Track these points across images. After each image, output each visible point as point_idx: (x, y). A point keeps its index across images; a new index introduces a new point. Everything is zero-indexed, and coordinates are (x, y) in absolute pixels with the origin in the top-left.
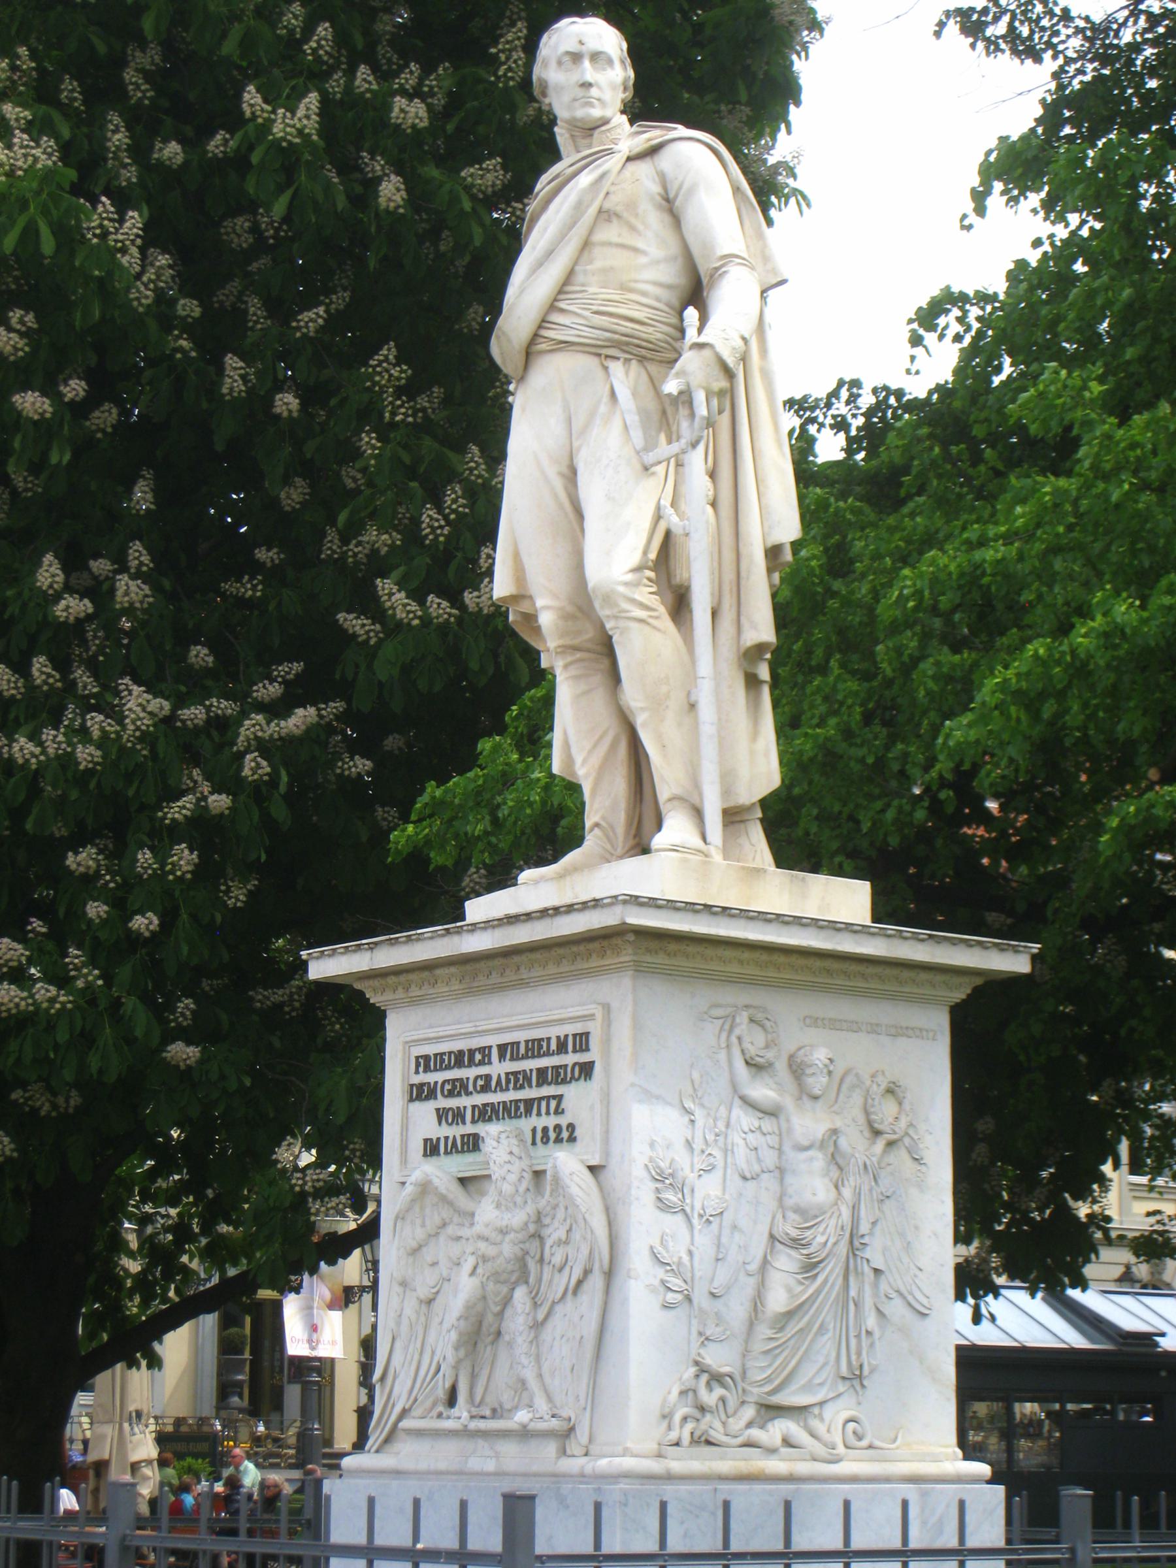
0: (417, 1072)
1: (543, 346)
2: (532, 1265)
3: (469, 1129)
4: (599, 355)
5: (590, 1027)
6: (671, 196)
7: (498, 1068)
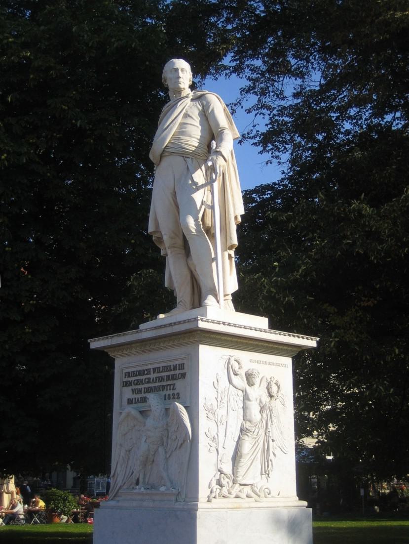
0: (125, 377)
1: (166, 154)
2: (165, 439)
3: (143, 395)
4: (183, 157)
5: (185, 361)
6: (205, 111)
7: (153, 376)
